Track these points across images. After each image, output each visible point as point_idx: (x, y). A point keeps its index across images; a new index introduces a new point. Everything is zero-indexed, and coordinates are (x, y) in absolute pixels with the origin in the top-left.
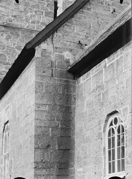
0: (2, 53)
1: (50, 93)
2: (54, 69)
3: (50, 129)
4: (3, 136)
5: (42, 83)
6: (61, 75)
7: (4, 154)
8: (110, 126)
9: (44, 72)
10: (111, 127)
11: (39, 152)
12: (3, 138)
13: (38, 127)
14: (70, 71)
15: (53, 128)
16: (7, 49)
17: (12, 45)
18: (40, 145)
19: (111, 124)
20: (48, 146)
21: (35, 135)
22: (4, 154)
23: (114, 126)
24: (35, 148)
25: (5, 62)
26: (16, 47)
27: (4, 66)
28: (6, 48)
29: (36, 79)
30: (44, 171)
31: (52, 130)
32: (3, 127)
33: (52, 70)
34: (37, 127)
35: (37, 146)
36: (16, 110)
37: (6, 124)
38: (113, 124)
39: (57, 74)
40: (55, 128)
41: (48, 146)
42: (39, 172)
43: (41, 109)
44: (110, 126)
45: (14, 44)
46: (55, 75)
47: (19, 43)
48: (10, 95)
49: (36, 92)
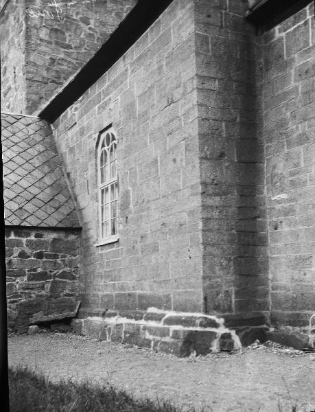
0: (59, 28)
1: (220, 56)
2: (223, 12)
3: (224, 124)
4: (96, 154)
5: (206, 38)
6: (235, 26)
7: (100, 185)
8: (102, 147)
9: (209, 16)
10: (104, 148)
11: (207, 164)
12: (96, 157)
13: (203, 119)
14: (249, 19)
15: (228, 122)
16: (66, 21)
17: (74, 14)
18: (208, 153)
19: (103, 146)
20: (222, 155)
21: (200, 134)
22: (100, 185)
23: (106, 148)
24: (201, 158)
25: (64, 44)
26: (81, 18)
27: (63, 49)
28: (65, 19)
29: (196, 29)
30: (218, 198)
31: (227, 127)
32: (97, 139)
33: (221, 14)
34: (203, 120)
35: (203, 155)
36: (135, 101)
37: (101, 132)
38: (106, 144)
39: (229, 22)
40: (231, 122)
41: (222, 155)
42: (210, 202)
43: (206, 86)
44: (102, 147)
45: (77, 14)
46: (226, 24)
47: (85, 11)
48: (112, 79)
49: (197, 54)
